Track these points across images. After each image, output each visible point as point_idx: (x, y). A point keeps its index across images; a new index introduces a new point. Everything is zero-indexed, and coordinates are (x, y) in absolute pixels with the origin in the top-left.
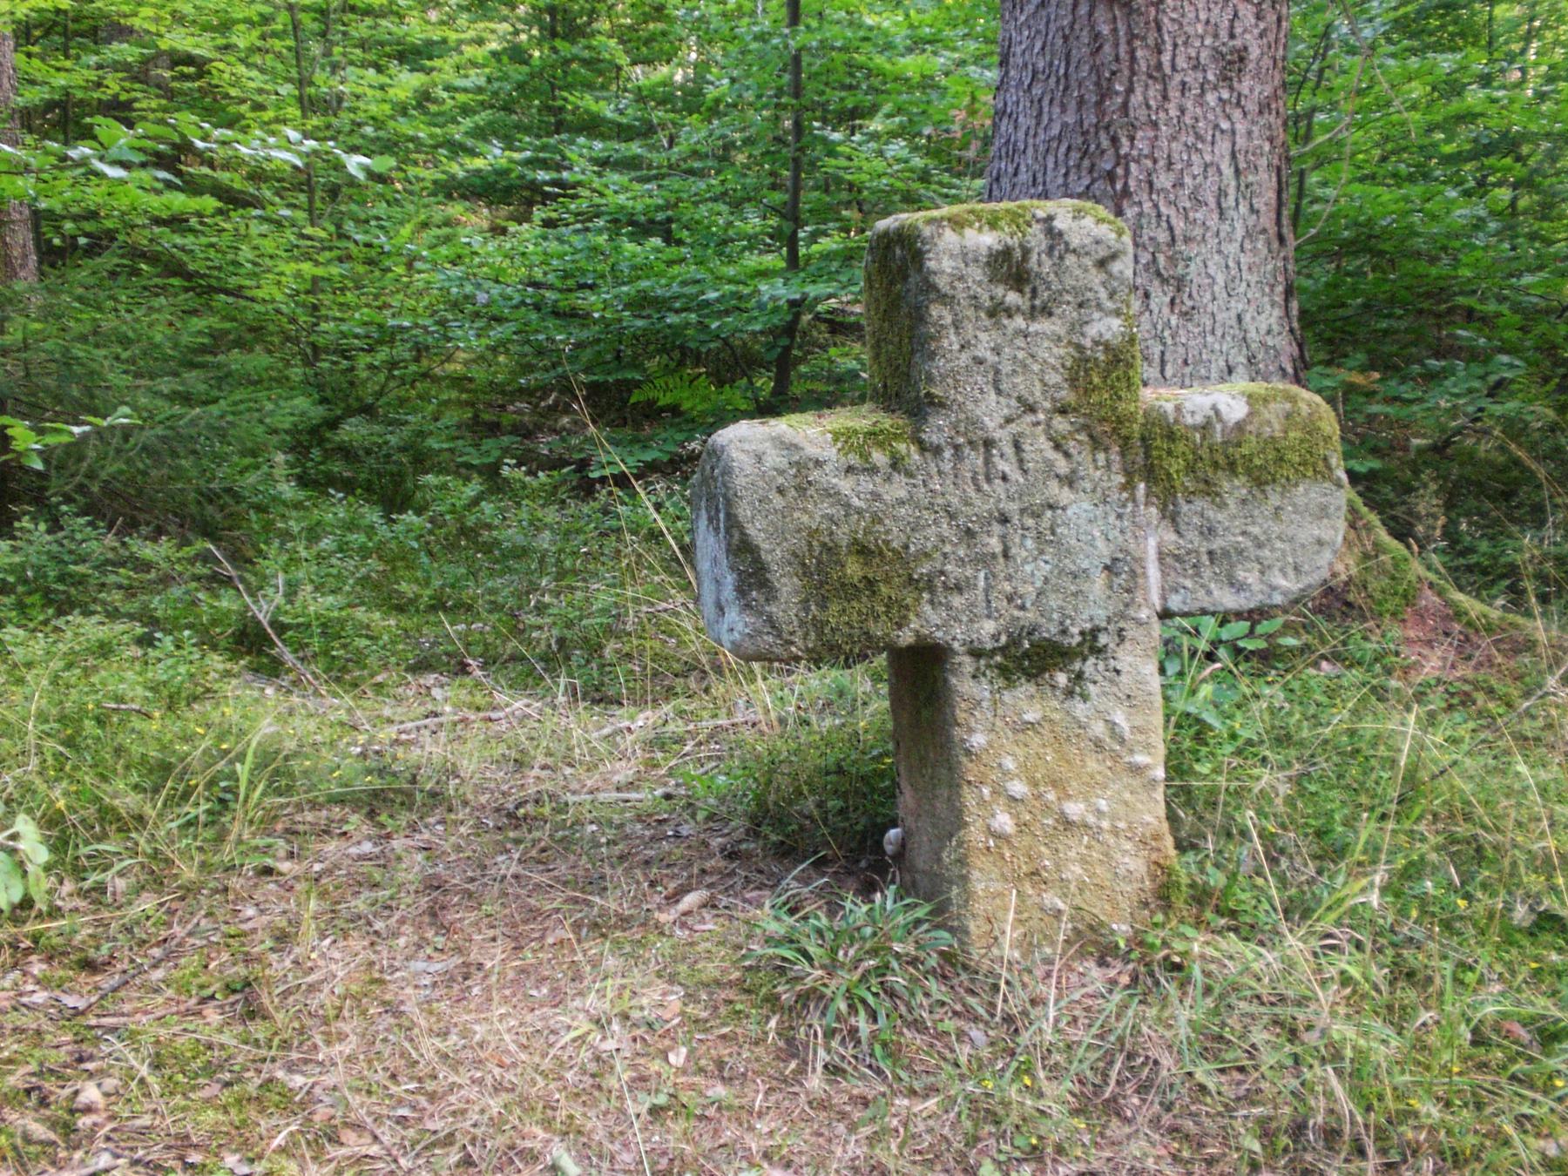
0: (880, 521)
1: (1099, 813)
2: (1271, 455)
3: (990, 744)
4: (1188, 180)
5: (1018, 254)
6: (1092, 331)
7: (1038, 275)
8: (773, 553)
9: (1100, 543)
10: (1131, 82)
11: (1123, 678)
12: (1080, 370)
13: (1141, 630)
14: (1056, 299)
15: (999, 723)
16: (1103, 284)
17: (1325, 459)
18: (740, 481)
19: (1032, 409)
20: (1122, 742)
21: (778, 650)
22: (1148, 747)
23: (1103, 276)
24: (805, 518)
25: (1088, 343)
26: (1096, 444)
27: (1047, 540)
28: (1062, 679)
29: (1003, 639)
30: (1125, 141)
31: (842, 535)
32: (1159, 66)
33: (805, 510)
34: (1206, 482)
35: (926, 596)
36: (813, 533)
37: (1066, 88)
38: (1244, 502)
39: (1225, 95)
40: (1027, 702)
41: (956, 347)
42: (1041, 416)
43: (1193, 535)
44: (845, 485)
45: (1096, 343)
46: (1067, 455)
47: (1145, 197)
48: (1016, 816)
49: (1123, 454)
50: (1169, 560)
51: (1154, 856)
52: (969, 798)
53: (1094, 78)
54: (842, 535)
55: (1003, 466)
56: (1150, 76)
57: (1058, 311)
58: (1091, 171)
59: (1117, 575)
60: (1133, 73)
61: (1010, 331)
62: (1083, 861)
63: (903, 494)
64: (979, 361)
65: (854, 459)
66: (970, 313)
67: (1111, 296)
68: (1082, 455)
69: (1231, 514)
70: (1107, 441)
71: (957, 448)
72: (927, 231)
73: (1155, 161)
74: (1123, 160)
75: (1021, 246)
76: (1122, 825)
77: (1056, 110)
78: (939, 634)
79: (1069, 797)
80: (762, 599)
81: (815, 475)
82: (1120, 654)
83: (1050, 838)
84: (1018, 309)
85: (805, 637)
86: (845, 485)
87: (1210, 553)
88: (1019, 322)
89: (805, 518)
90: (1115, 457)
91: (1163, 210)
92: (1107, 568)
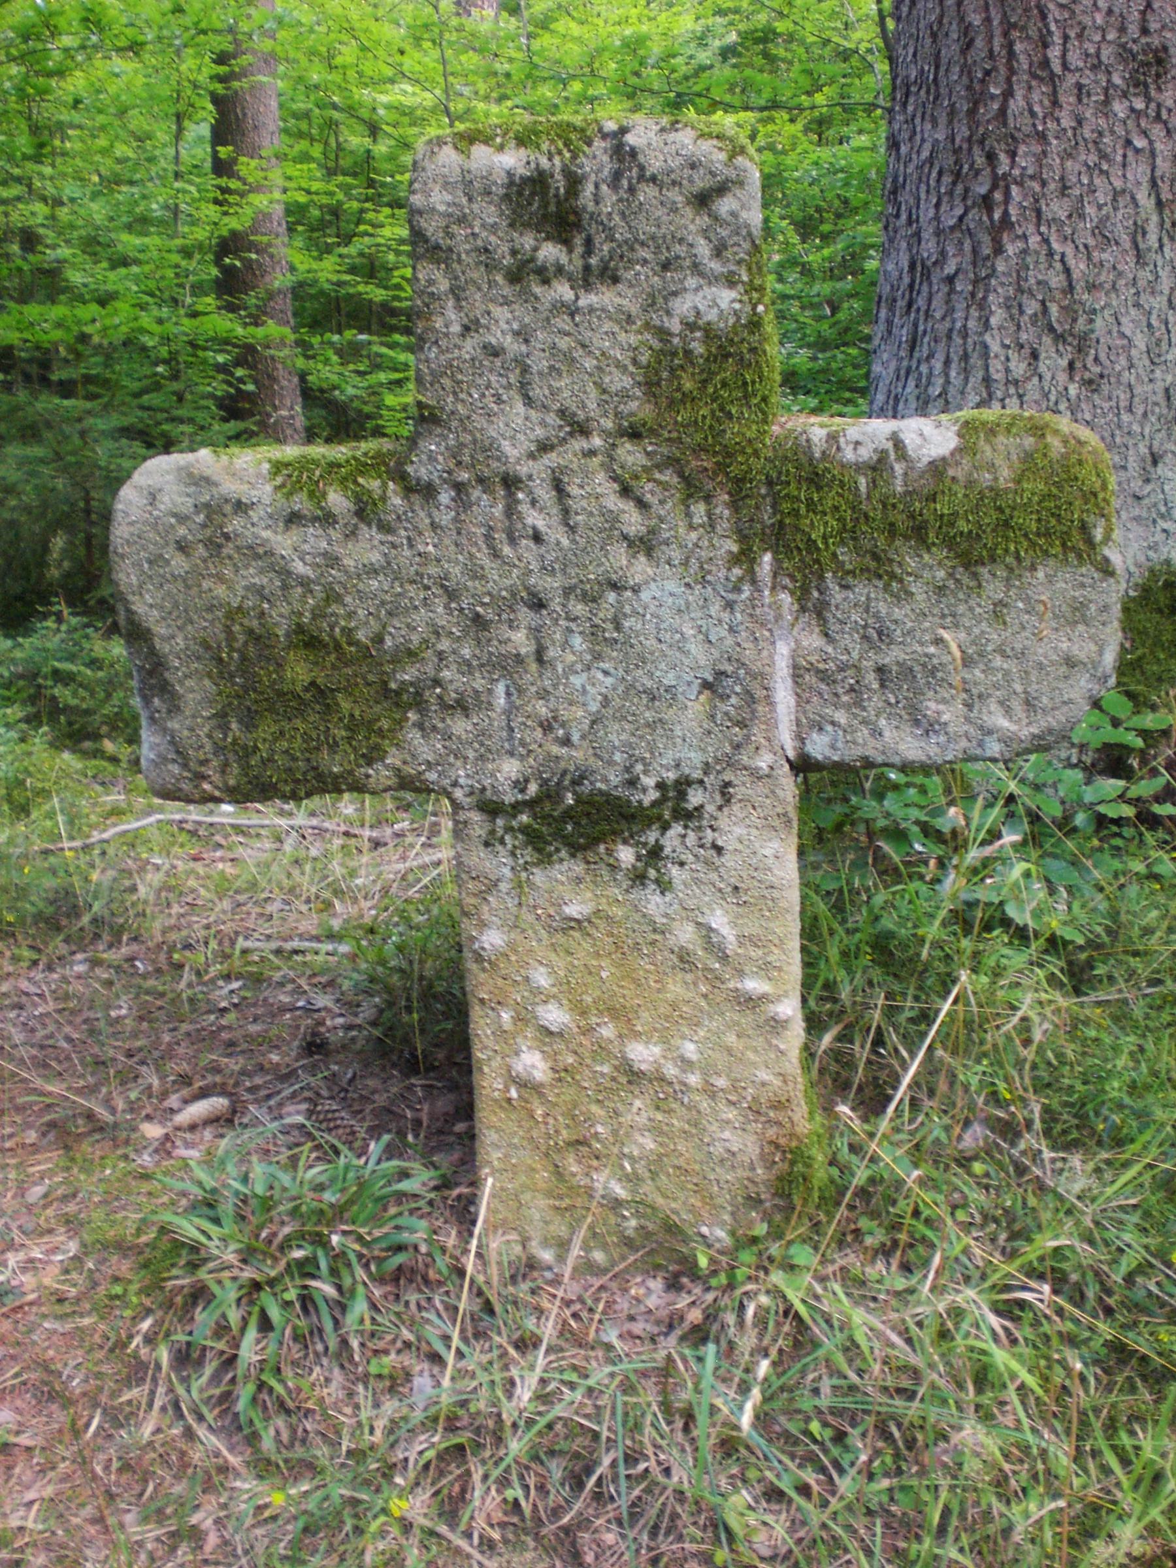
0: (339, 599)
1: (686, 1064)
2: (990, 518)
3: (512, 946)
4: (1090, 210)
5: (559, 183)
6: (683, 306)
9: (695, 648)
10: (1008, 80)
11: (728, 860)
12: (663, 368)
13: (761, 788)
14: (625, 252)
15: (527, 917)
16: (705, 233)
17: (1084, 528)
19: (582, 429)
20: (724, 958)
21: (186, 786)
22: (766, 969)
23: (704, 220)
24: (221, 591)
25: (675, 326)
26: (691, 489)
27: (606, 639)
28: (626, 855)
29: (533, 788)
30: (1003, 158)
31: (280, 618)
32: (1045, 63)
33: (220, 578)
34: (876, 557)
35: (412, 716)
37: (936, 98)
38: (941, 590)
39: (1139, 105)
40: (568, 888)
41: (456, 328)
42: (597, 442)
44: (284, 543)
45: (691, 327)
46: (642, 505)
47: (1031, 229)
48: (552, 1057)
49: (735, 505)
51: (771, 1132)
54: (280, 618)
55: (534, 519)
56: (1034, 76)
59: (724, 697)
63: (375, 557)
64: (494, 352)
65: (301, 502)
67: (719, 251)
68: (667, 508)
69: (925, 615)
71: (459, 487)
73: (1044, 184)
75: (567, 173)
76: (721, 1082)
79: (637, 1035)
81: (235, 524)
82: (723, 822)
83: (603, 1095)
84: (560, 270)
85: (224, 769)
86: (284, 543)
87: (880, 670)
88: (563, 291)
89: (221, 591)
91: (1055, 246)
92: (706, 685)
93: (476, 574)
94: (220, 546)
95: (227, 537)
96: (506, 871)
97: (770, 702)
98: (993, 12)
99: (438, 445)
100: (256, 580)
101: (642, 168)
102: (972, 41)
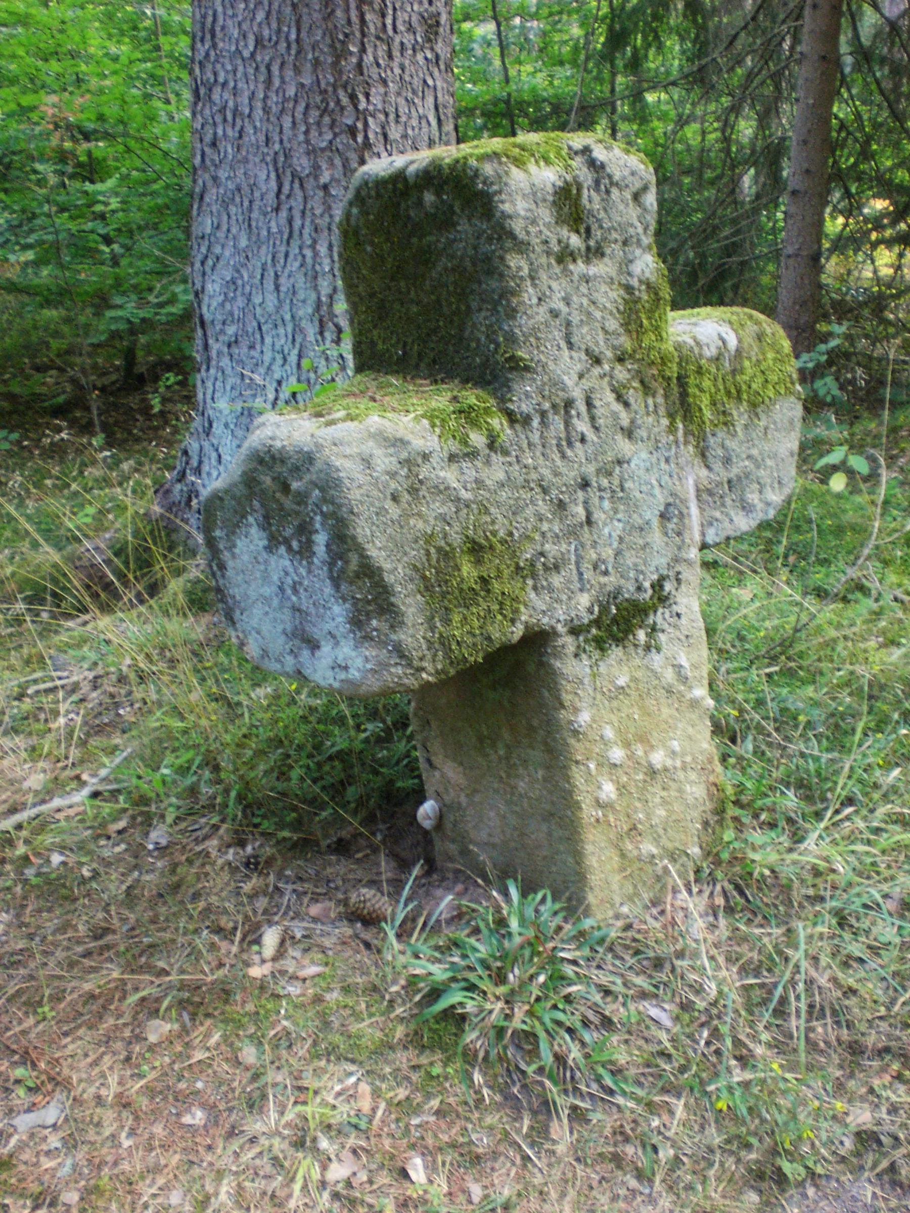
7: (590, 212)
8: (395, 571)
9: (657, 491)
10: (363, 44)
11: (684, 621)
18: (355, 495)
24: (420, 525)
25: (635, 282)
26: (647, 389)
29: (596, 609)
30: (361, 97)
33: (419, 515)
35: (530, 582)
36: (429, 538)
37: (299, 52)
40: (619, 667)
41: (535, 301)
43: (717, 466)
44: (450, 476)
46: (626, 405)
50: (705, 496)
52: (578, 776)
53: (328, 40)
56: (378, 38)
57: (608, 251)
58: (332, 126)
60: (363, 35)
61: (576, 278)
62: (664, 802)
64: (555, 314)
66: (543, 260)
70: (654, 384)
71: (543, 414)
72: (488, 169)
74: (362, 115)
76: (688, 759)
77: (289, 73)
78: (545, 620)
80: (385, 627)
86: (450, 476)
89: (420, 525)
90: (660, 400)
93: (556, 474)
94: (417, 490)
95: (421, 482)
96: (588, 670)
97: (689, 515)
100: (441, 511)
101: (610, 177)
102: (333, 11)
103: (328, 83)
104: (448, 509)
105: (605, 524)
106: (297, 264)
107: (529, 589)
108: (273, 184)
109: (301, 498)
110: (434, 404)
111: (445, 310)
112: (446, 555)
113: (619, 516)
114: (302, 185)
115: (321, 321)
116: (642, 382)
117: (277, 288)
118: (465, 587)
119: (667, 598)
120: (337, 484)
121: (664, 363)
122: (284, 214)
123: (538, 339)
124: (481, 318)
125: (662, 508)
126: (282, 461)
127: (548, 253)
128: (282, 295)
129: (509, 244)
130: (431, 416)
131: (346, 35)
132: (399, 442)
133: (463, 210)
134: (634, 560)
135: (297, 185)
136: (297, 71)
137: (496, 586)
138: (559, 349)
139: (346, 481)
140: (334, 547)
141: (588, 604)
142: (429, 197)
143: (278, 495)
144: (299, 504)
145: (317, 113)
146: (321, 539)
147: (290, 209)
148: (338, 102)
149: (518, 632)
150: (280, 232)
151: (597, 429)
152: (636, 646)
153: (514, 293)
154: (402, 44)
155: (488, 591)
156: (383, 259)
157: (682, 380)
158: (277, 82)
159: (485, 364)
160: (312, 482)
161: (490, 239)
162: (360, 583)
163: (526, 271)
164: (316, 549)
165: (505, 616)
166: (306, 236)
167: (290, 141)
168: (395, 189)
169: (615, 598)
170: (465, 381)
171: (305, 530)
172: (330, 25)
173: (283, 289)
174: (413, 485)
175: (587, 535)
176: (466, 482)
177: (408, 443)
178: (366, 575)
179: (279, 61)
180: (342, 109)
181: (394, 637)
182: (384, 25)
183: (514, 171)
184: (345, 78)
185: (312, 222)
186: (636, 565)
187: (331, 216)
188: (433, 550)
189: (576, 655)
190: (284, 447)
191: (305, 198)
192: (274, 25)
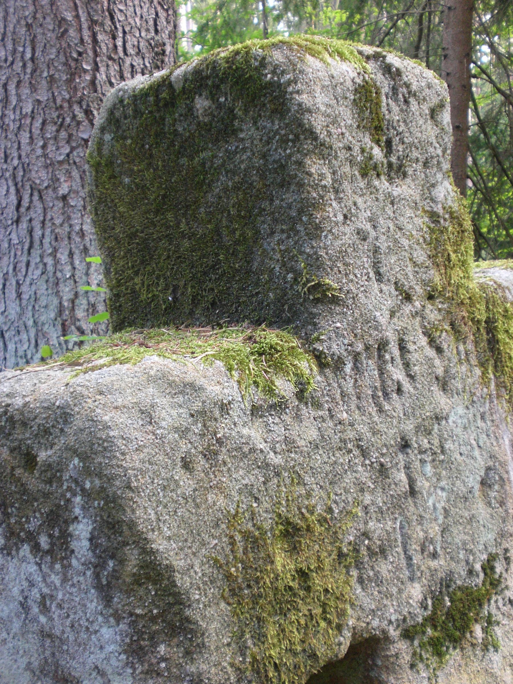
8: (190, 568)
9: (477, 453)
10: (96, 63)
18: (133, 461)
24: (221, 502)
25: (439, 209)
29: (430, 602)
33: (219, 488)
35: (354, 573)
37: (34, 71)
41: (340, 218)
44: (254, 433)
46: (439, 350)
53: (62, 59)
56: (110, 58)
66: (347, 169)
70: (465, 329)
71: (356, 356)
77: (25, 91)
78: (375, 623)
86: (254, 433)
89: (221, 502)
90: (470, 346)
94: (216, 454)
95: (219, 441)
98: (81, 12)
99: (341, 322)
101: (408, 86)
102: (66, 31)
103: (63, 100)
104: (254, 478)
105: (430, 494)
106: (38, 272)
107: (353, 581)
108: (13, 198)
109: (53, 473)
110: (225, 345)
111: (227, 240)
112: (254, 541)
113: (443, 483)
114: (41, 197)
115: (63, 325)
116: (452, 324)
117: (19, 295)
118: (280, 585)
119: (499, 581)
120: (106, 446)
121: (472, 305)
122: (24, 225)
123: (346, 264)
124: (273, 245)
125: (482, 473)
126: (24, 424)
127: (352, 162)
128: (24, 302)
129: (308, 146)
130: (226, 356)
131: (80, 54)
132: (191, 388)
133: (246, 111)
134: (462, 536)
135: (36, 197)
136: (34, 88)
137: (317, 581)
138: (369, 279)
139: (120, 442)
140: (103, 541)
141: (420, 597)
142: (201, 103)
143: (18, 472)
144: (50, 482)
145: (54, 128)
146: (82, 530)
147: (30, 220)
148: (74, 117)
149: (345, 641)
150: (21, 243)
151: (412, 377)
152: (473, 645)
153: (316, 206)
154: (132, 66)
155: (308, 589)
156: (144, 188)
157: (490, 326)
158: (14, 100)
159: (281, 300)
160: (68, 448)
161: (284, 141)
162: (141, 592)
163: (328, 181)
164: (74, 545)
165: (329, 622)
166: (46, 245)
167: (28, 156)
168: (157, 100)
169: (448, 586)
170: (258, 323)
171: (58, 520)
172: (64, 45)
173: (25, 296)
174: (209, 446)
175: (412, 509)
176: (274, 442)
177: (201, 389)
178: (148, 578)
179: (15, 80)
180: (79, 123)
181: (192, 668)
182: (115, 47)
183: (309, 58)
184: (79, 94)
185: (52, 231)
186: (464, 544)
187: (71, 226)
188: (238, 537)
189: (412, 666)
190: (26, 404)
191: (45, 209)
192: (10, 47)
